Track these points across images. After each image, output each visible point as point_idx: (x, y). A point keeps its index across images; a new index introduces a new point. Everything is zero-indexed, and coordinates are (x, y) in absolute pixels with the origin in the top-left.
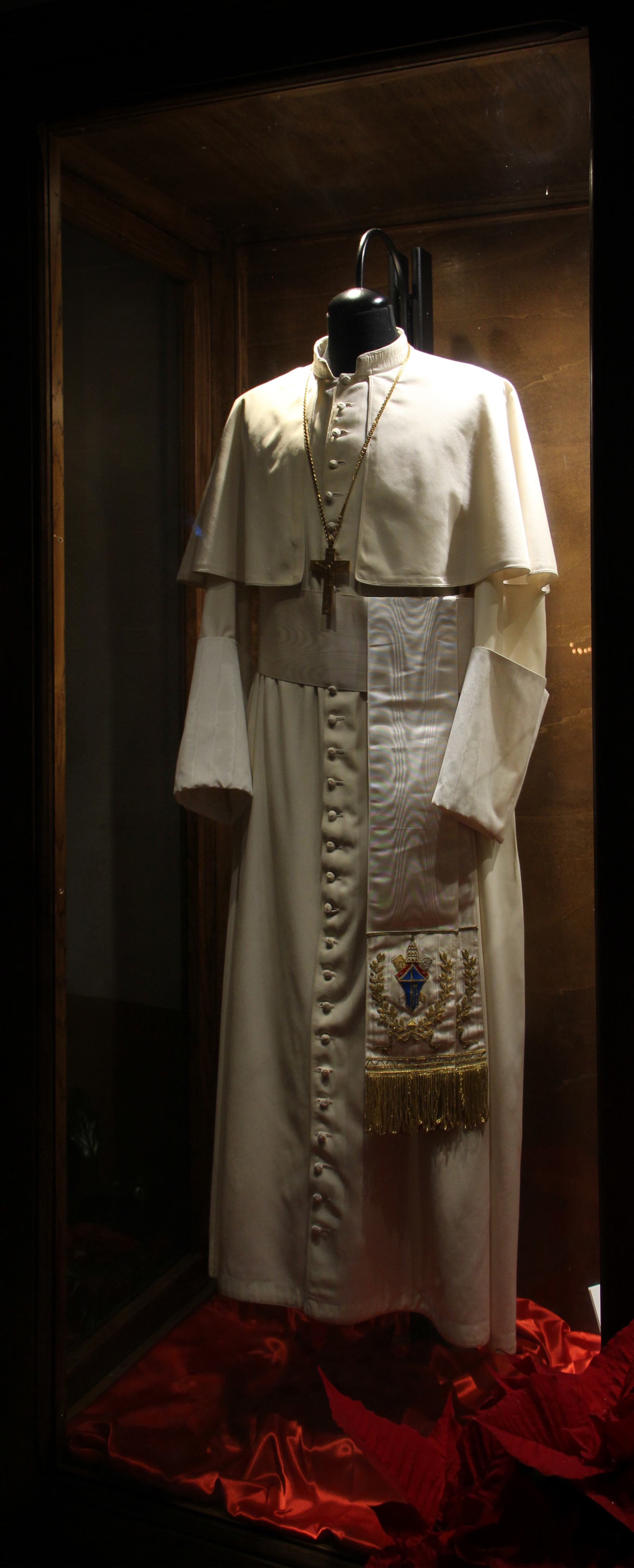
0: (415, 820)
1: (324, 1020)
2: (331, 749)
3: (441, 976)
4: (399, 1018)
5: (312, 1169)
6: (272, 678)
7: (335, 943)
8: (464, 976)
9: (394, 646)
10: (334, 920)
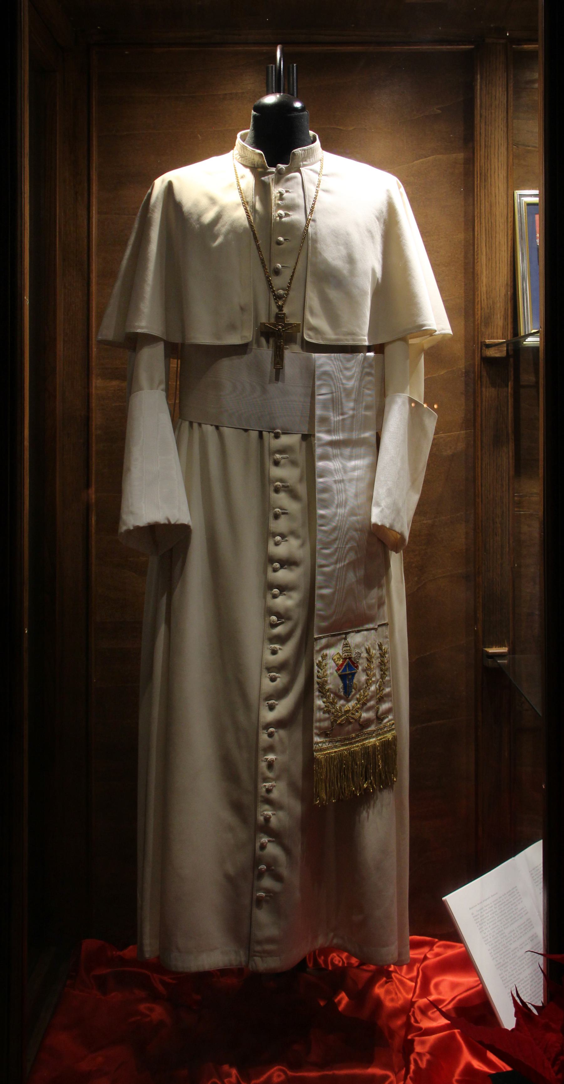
0: (352, 538)
1: (269, 716)
2: (278, 483)
3: (366, 666)
4: (338, 706)
5: (258, 845)
6: (212, 425)
7: (280, 649)
8: (380, 664)
9: (334, 394)
10: (279, 630)
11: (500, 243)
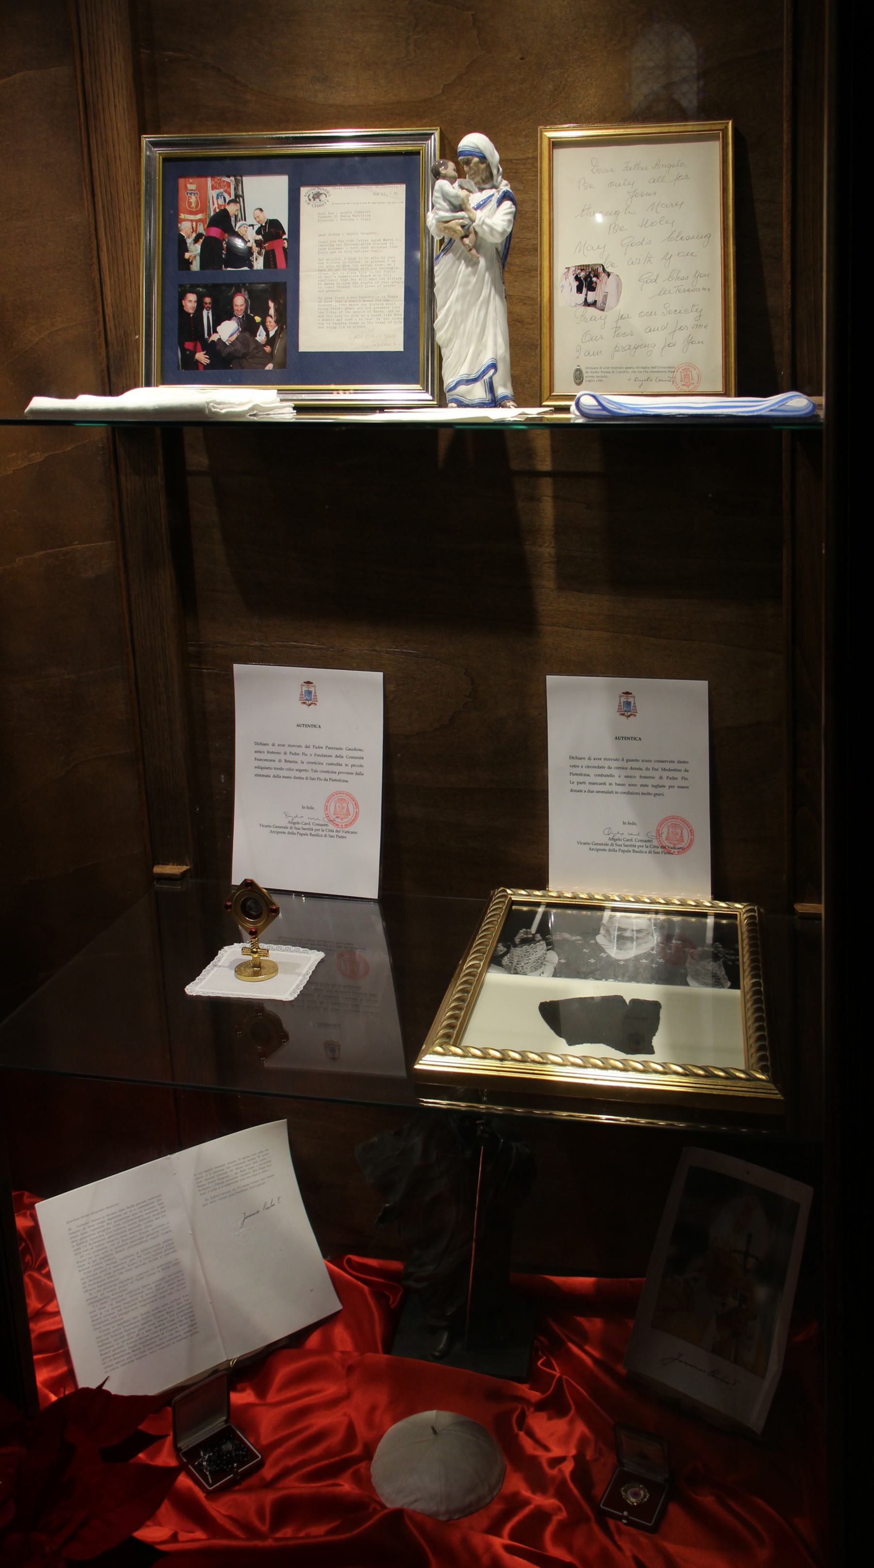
11: (127, 230)
